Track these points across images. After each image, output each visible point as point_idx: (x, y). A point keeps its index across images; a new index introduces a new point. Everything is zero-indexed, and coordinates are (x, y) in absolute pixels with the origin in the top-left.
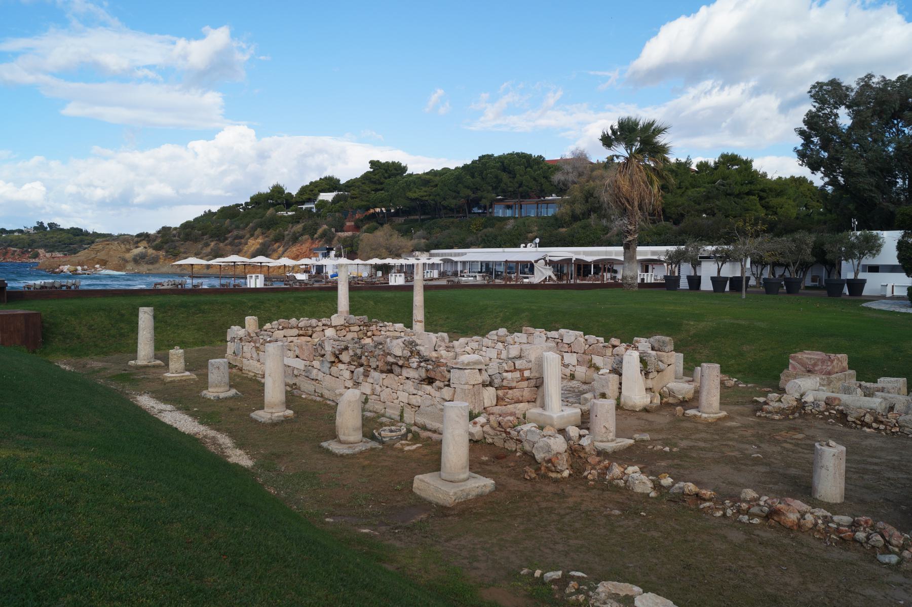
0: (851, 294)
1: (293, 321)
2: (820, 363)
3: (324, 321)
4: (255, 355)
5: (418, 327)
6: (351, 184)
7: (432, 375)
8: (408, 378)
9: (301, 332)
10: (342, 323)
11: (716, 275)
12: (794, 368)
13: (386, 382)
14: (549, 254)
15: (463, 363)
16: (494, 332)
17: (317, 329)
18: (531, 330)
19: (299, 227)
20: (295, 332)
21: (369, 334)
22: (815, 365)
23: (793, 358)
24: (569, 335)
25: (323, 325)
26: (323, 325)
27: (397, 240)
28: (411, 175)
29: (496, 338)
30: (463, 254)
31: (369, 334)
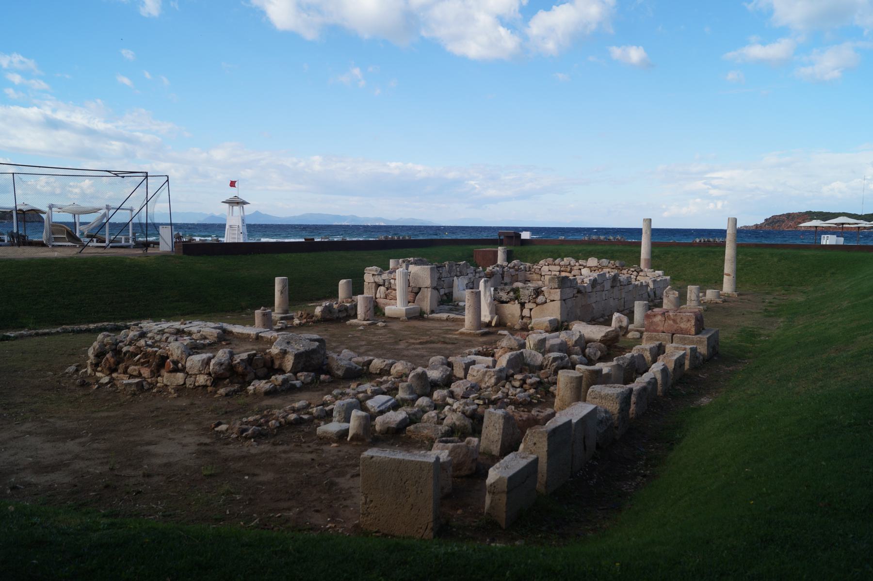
3: (581, 262)
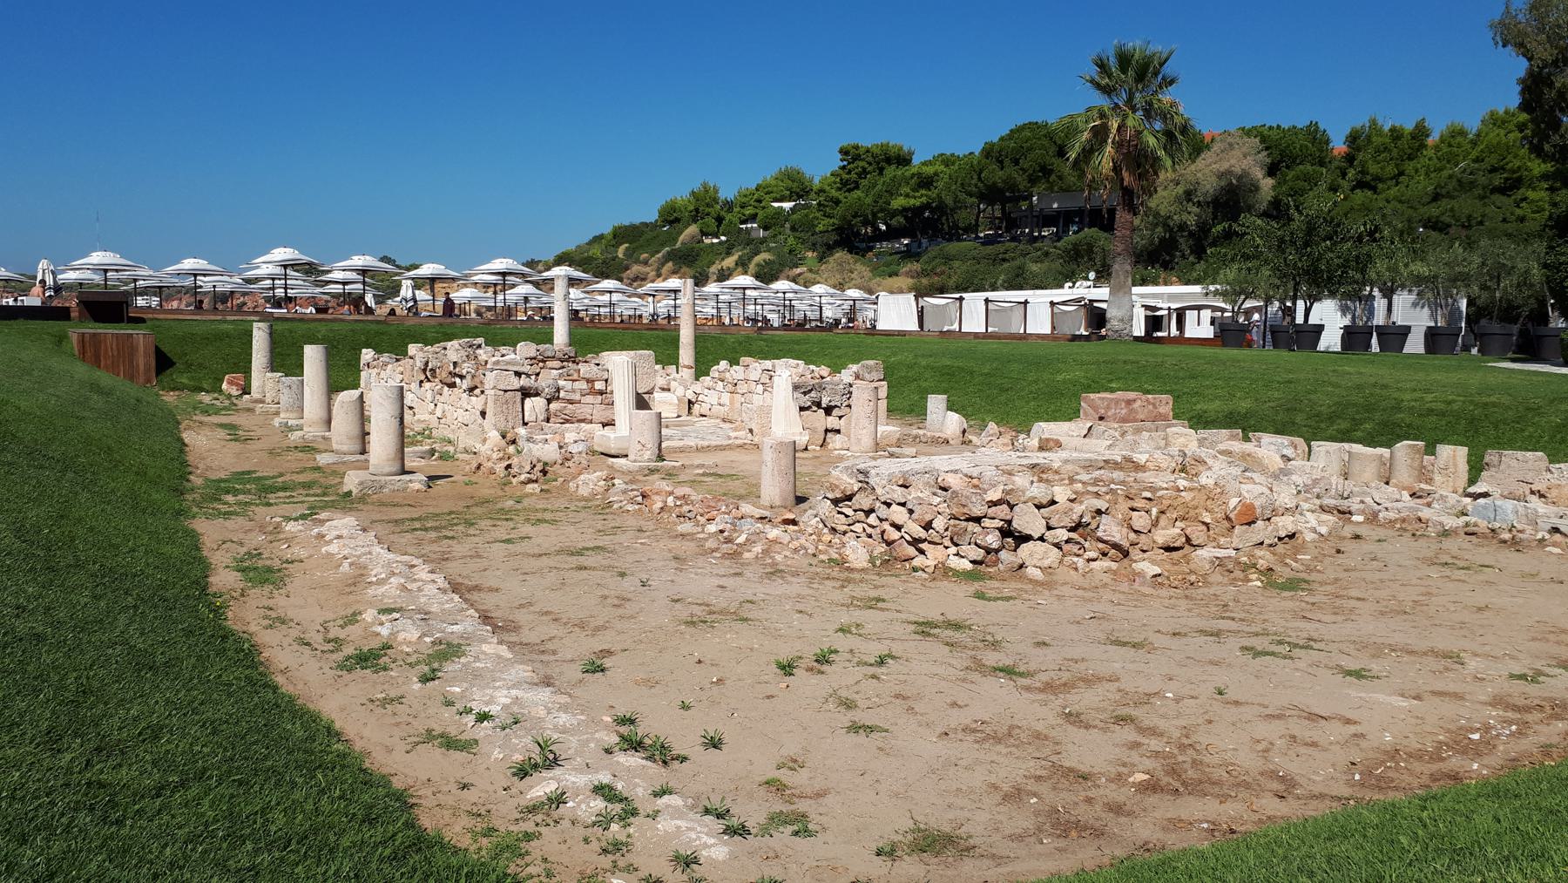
19: (730, 262)
22: (1108, 408)
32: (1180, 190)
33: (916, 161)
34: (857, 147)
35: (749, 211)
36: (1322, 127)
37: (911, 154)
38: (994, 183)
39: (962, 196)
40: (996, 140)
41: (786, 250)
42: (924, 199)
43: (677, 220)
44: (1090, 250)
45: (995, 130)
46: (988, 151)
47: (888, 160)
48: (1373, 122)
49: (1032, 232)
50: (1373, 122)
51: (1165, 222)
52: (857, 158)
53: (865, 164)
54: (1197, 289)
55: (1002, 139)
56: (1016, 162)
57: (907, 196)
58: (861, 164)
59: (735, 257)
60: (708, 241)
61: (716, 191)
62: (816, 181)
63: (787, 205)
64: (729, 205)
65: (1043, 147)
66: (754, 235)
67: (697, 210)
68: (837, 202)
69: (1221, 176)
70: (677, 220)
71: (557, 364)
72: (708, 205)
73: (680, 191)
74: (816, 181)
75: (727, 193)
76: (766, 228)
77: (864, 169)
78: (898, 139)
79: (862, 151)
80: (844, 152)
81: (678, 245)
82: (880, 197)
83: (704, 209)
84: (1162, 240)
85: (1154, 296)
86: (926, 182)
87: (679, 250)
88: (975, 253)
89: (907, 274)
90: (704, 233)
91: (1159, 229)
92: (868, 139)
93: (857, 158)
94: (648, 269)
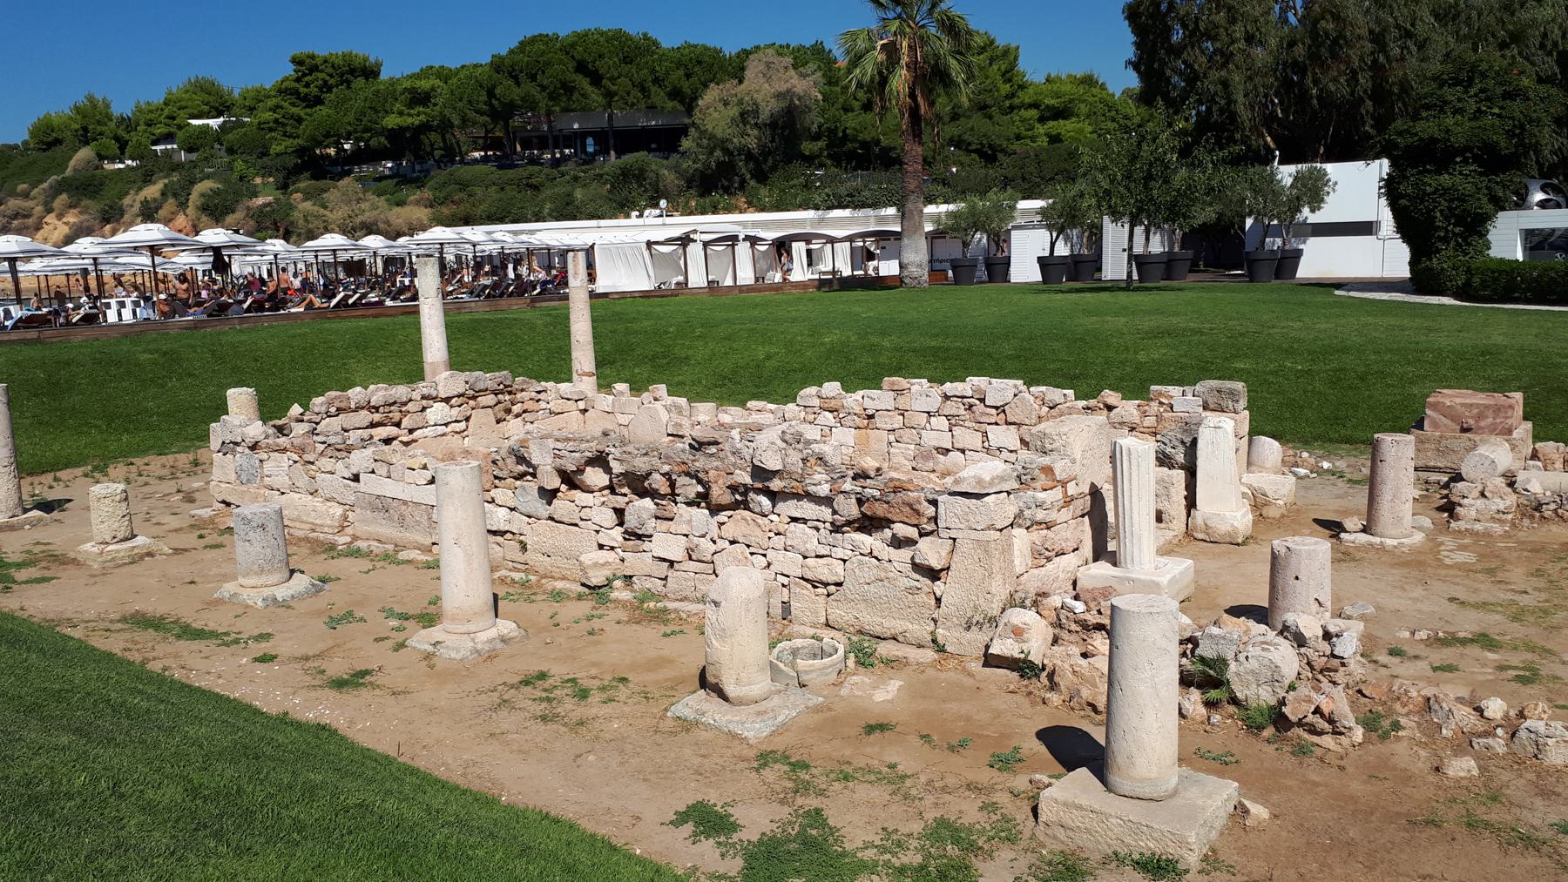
0: (1141, 280)
1: (356, 394)
2: (1490, 413)
4: (302, 482)
5: (586, 385)
6: (253, 102)
7: (880, 510)
8: (794, 520)
9: (377, 417)
10: (461, 390)
11: (1047, 253)
12: (1435, 425)
13: (730, 531)
14: (700, 228)
15: (980, 482)
16: (812, 390)
17: (410, 406)
18: (901, 382)
19: (152, 191)
20: (365, 417)
21: (516, 409)
22: (1480, 417)
23: (1435, 406)
24: (1001, 389)
25: (423, 397)
26: (423, 397)
27: (373, 206)
28: (393, 82)
29: (816, 402)
30: (532, 232)
31: (516, 409)
32: (734, 111)
33: (384, 75)
34: (313, 57)
35: (160, 130)
36: (99, 97)
37: (379, 65)
38: (512, 101)
39: (471, 114)
40: (504, 52)
41: (236, 176)
42: (422, 117)
43: (58, 142)
44: (642, 171)
45: (503, 44)
46: (498, 65)
47: (352, 71)
48: (91, 99)
49: (553, 154)
50: (91, 99)
51: (723, 144)
52: (314, 69)
53: (318, 80)
54: (810, 214)
55: (511, 52)
56: (533, 78)
57: (401, 114)
58: (321, 75)
59: (159, 186)
60: (108, 166)
61: (108, 106)
62: (236, 94)
63: (214, 123)
64: (128, 124)
65: (561, 62)
66: (175, 158)
67: (85, 129)
68: (299, 120)
69: (779, 96)
70: (58, 142)
71: (490, 399)
72: (99, 123)
73: (59, 104)
74: (236, 94)
75: (122, 107)
76: (190, 150)
77: (325, 82)
78: (364, 48)
79: (319, 61)
80: (297, 61)
81: (69, 172)
82: (363, 114)
83: (91, 125)
84: (719, 164)
85: (755, 224)
86: (420, 98)
87: (73, 179)
88: (494, 177)
89: (417, 203)
90: (101, 158)
91: (718, 153)
92: (328, 45)
93: (314, 69)
94: (30, 204)
